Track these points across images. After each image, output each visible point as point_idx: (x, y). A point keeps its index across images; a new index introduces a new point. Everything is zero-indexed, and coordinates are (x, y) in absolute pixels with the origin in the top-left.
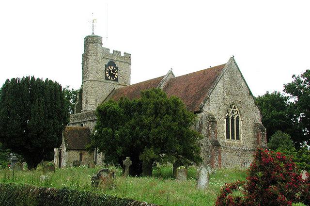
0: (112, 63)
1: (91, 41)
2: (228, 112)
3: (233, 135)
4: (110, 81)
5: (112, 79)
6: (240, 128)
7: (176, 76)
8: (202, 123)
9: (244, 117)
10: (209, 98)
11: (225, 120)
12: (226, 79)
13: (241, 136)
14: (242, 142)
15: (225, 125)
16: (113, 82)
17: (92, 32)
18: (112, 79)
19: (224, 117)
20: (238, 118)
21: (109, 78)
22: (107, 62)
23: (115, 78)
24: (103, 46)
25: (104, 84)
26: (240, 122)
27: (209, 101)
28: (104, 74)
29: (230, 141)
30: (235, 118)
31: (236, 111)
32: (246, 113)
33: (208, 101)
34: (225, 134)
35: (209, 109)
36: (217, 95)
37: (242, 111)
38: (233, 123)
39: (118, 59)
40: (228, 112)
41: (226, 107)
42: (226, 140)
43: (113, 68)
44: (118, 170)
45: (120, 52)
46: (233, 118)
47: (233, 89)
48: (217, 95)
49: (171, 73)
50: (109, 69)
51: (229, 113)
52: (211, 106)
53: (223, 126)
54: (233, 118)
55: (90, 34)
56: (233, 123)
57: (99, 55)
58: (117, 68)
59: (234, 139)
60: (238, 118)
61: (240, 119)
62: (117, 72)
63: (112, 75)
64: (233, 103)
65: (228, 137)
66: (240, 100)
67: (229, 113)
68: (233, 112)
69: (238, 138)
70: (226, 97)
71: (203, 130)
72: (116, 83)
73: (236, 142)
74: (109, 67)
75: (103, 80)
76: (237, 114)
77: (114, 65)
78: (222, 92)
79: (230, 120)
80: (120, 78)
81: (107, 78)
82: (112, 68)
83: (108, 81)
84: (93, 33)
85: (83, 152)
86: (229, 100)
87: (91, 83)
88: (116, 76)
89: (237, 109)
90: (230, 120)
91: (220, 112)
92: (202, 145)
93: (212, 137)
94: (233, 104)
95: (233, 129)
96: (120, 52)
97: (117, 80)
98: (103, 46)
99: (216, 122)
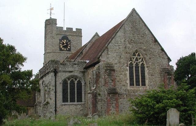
0: (65, 38)
1: (50, 23)
2: (131, 60)
3: (138, 82)
4: (64, 52)
5: (65, 49)
6: (146, 74)
7: (100, 36)
8: (99, 73)
9: (150, 64)
10: (107, 48)
11: (128, 68)
12: (127, 29)
13: (147, 82)
14: (148, 88)
15: (128, 73)
16: (66, 52)
17: (50, 17)
18: (65, 49)
19: (126, 65)
20: (143, 64)
21: (63, 49)
22: (60, 37)
23: (68, 48)
24: (57, 26)
25: (58, 54)
26: (146, 69)
27: (108, 50)
28: (58, 46)
29: (135, 88)
30: (140, 65)
31: (140, 59)
32: (152, 59)
33: (106, 51)
34: (128, 82)
35: (108, 58)
36: (116, 45)
37: (147, 58)
38: (137, 71)
39: (70, 34)
40: (131, 60)
41: (128, 55)
42: (129, 87)
43: (66, 41)
44: (160, 104)
45: (72, 29)
46: (137, 64)
47: (136, 38)
48: (116, 45)
49: (97, 34)
50: (62, 42)
51: (132, 61)
52: (110, 56)
53: (125, 74)
54: (137, 64)
55: (49, 18)
56: (137, 71)
57: (54, 32)
58: (70, 41)
59: (139, 85)
60: (143, 64)
61: (145, 66)
62: (69, 44)
63: (66, 47)
64: (136, 50)
65: (132, 84)
66: (145, 48)
67: (132, 61)
68: (137, 59)
69: (144, 84)
70: (128, 45)
71: (100, 79)
72: (69, 52)
73: (141, 88)
74: (63, 41)
75: (58, 51)
76: (142, 61)
77: (67, 39)
78: (122, 41)
79: (134, 68)
80: (72, 48)
81: (61, 50)
82: (65, 41)
83: (62, 52)
84: (51, 17)
85: (29, 108)
86: (132, 48)
87: (48, 55)
88: (69, 47)
89: (141, 57)
90: (134, 68)
91: (122, 60)
92: (99, 95)
93: (111, 85)
94: (136, 51)
95: (137, 76)
96: (72, 29)
97: (70, 50)
98: (57, 26)
99: (114, 70)
